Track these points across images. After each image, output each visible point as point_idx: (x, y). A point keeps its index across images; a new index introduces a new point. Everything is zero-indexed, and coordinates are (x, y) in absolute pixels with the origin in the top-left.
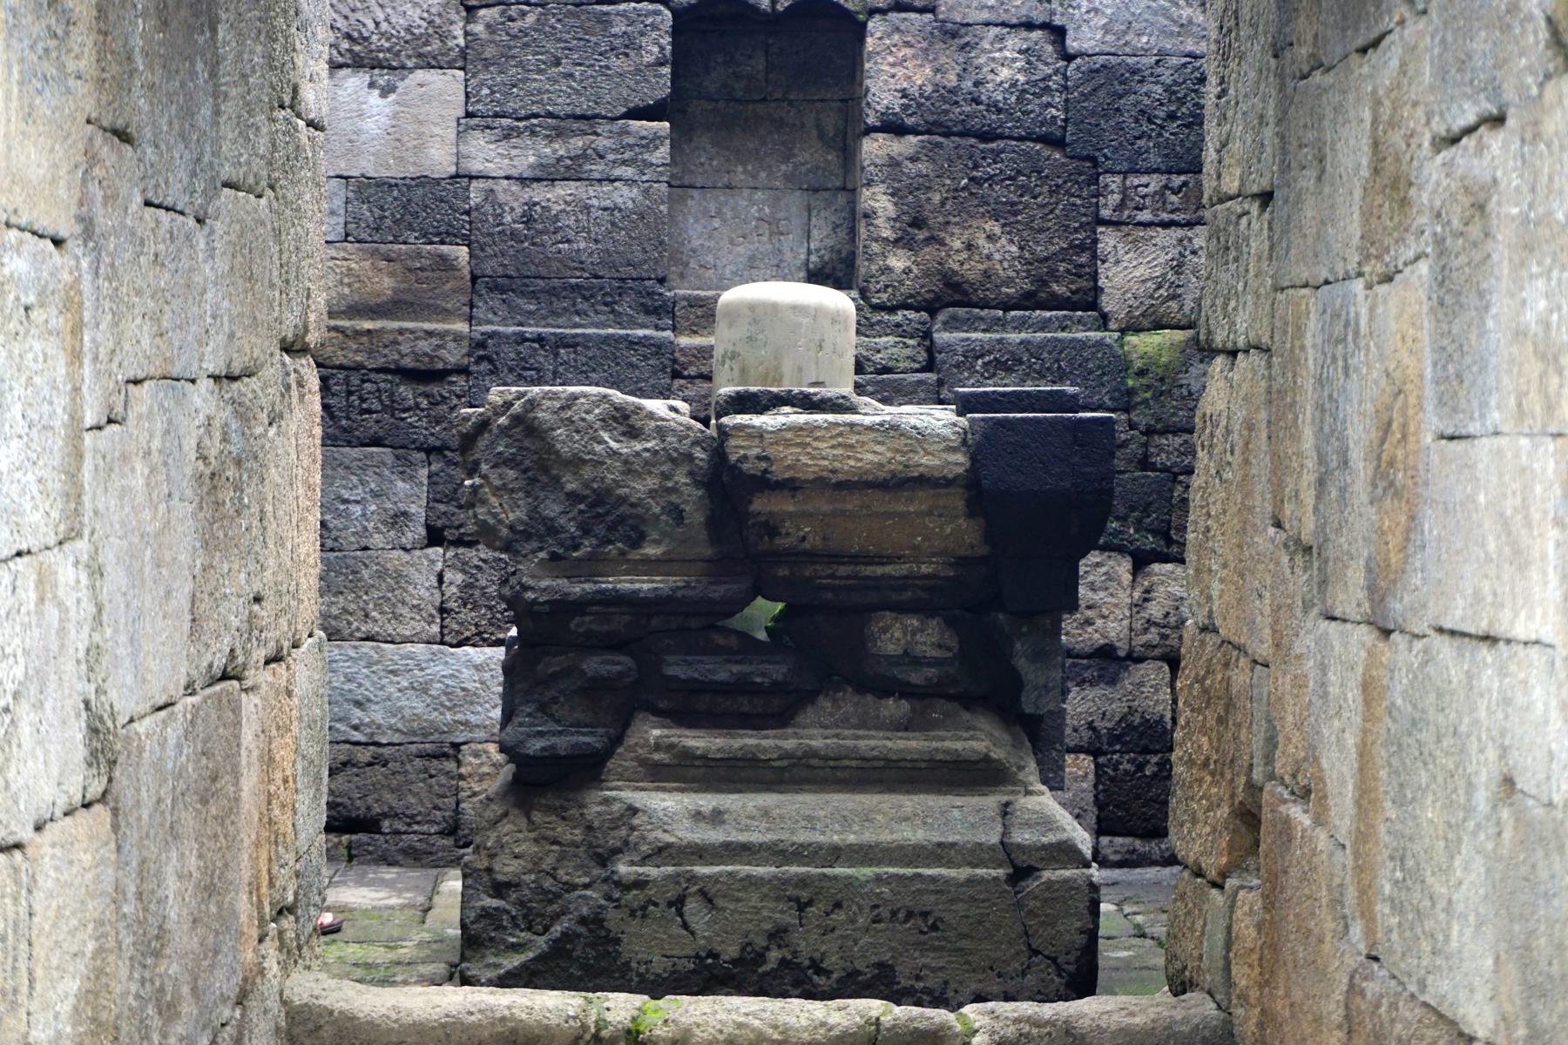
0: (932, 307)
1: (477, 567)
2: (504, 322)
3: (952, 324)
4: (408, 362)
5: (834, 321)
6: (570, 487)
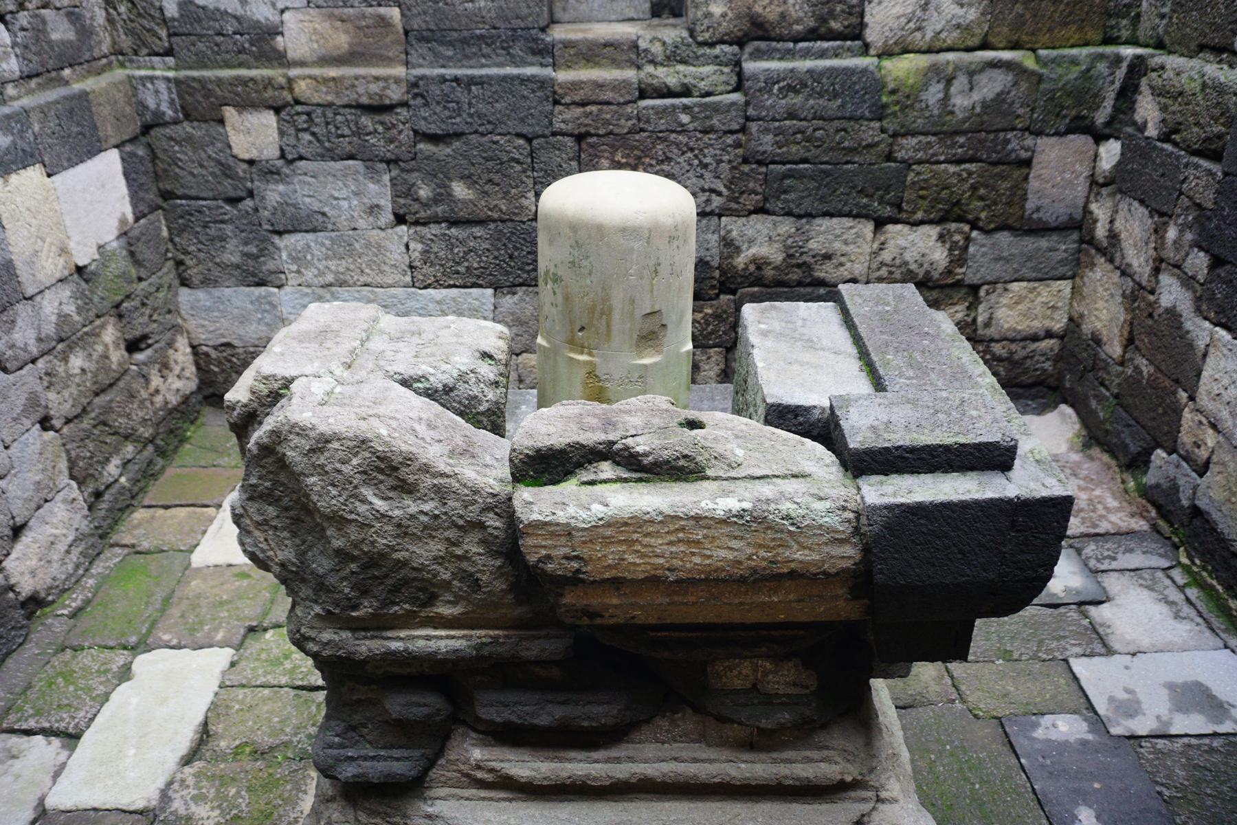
0: (741, 43)
1: (432, 240)
2: (431, 65)
3: (757, 55)
4: (365, 100)
5: (672, 238)
6: (338, 543)
